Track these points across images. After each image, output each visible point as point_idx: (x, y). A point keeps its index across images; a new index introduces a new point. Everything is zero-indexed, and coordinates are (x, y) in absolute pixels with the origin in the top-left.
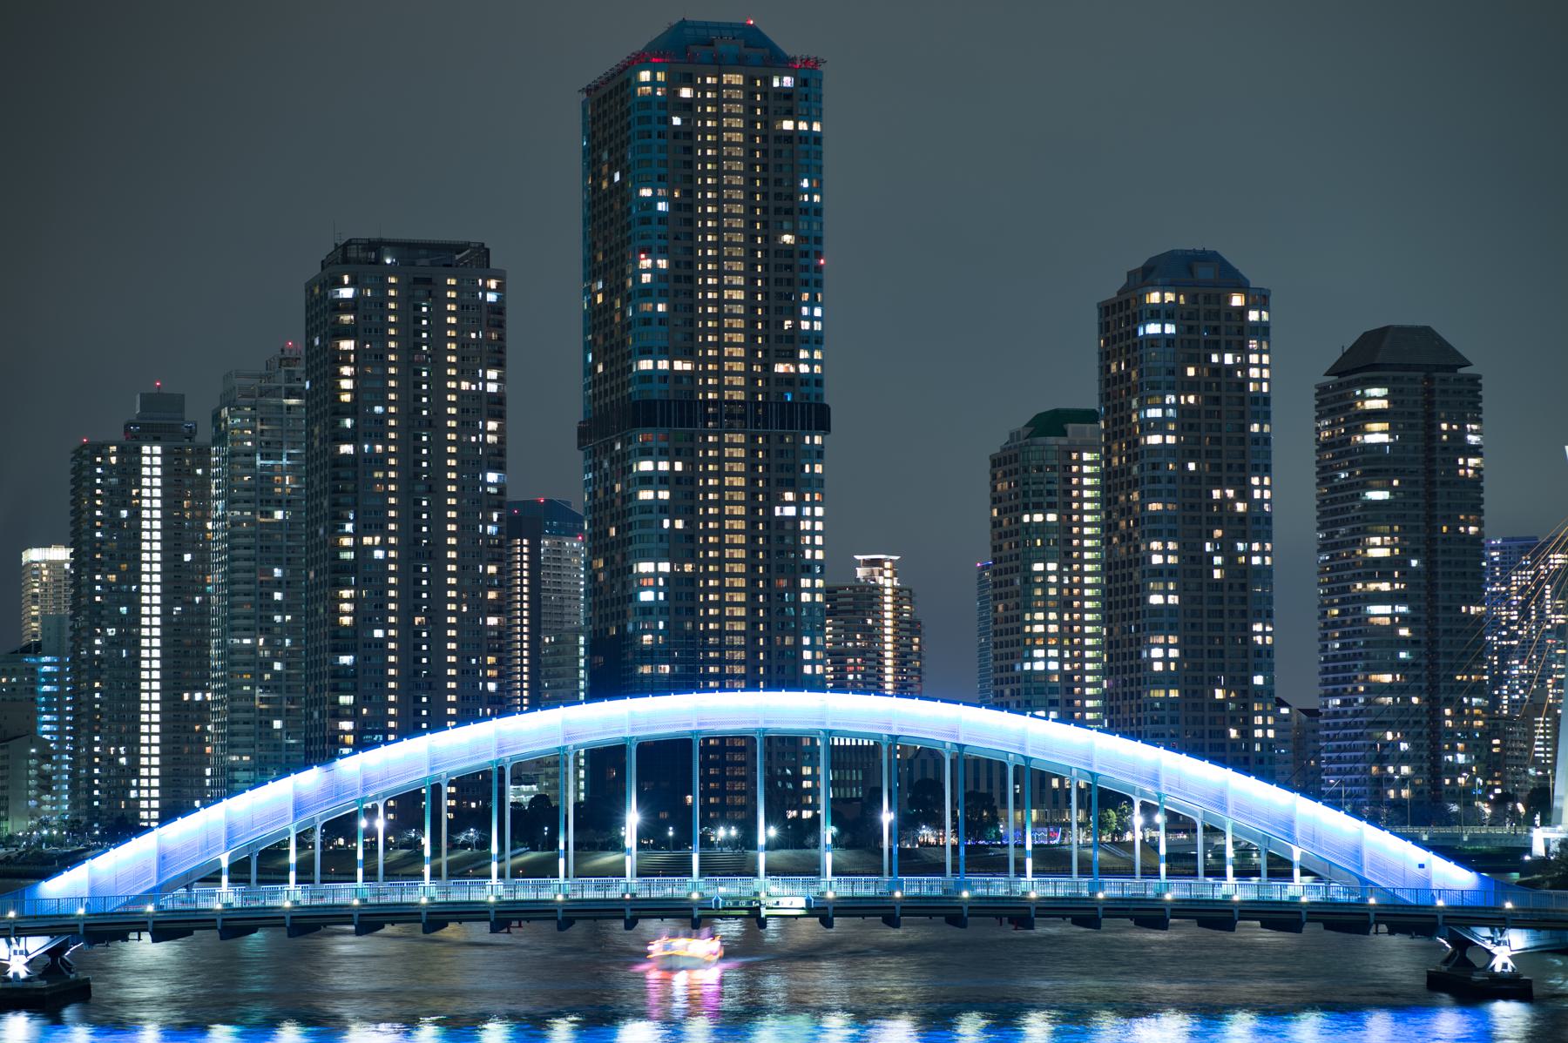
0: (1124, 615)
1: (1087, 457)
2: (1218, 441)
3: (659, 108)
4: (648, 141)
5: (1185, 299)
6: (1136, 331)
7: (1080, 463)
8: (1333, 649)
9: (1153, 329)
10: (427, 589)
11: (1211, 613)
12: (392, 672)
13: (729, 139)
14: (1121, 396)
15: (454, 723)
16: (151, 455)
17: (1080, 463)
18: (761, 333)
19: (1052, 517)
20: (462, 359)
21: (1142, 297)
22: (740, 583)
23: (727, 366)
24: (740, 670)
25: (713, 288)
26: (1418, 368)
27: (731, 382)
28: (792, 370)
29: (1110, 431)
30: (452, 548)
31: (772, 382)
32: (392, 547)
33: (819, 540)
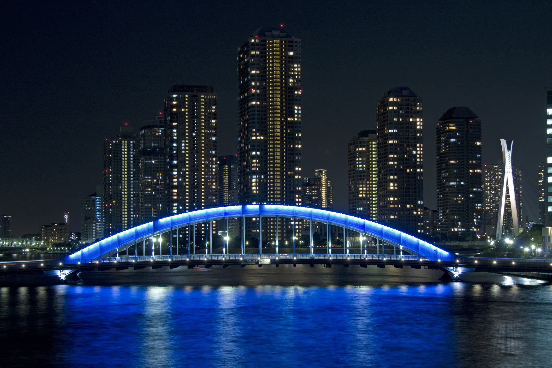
0: (383, 213)
1: (373, 143)
2: (409, 185)
3: (257, 115)
4: (254, 113)
5: (400, 100)
6: (386, 109)
7: (372, 144)
8: (441, 197)
9: (391, 108)
10: (197, 196)
11: (406, 105)
12: (187, 204)
13: (276, 54)
14: (382, 134)
15: (204, 208)
16: (124, 143)
17: (372, 144)
18: (285, 137)
19: (364, 149)
20: (206, 148)
21: (388, 99)
22: (279, 169)
23: (275, 126)
24: (279, 200)
25: (271, 63)
26: (463, 118)
27: (276, 115)
28: (293, 120)
29: (379, 125)
30: (203, 189)
31: (287, 123)
32: (187, 150)
33: (299, 116)
